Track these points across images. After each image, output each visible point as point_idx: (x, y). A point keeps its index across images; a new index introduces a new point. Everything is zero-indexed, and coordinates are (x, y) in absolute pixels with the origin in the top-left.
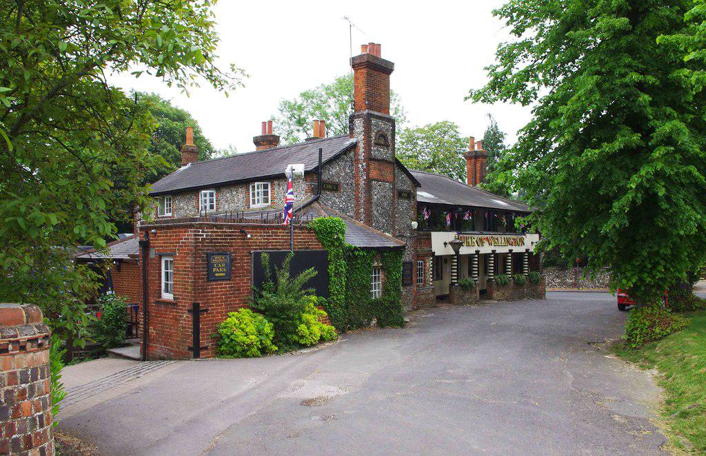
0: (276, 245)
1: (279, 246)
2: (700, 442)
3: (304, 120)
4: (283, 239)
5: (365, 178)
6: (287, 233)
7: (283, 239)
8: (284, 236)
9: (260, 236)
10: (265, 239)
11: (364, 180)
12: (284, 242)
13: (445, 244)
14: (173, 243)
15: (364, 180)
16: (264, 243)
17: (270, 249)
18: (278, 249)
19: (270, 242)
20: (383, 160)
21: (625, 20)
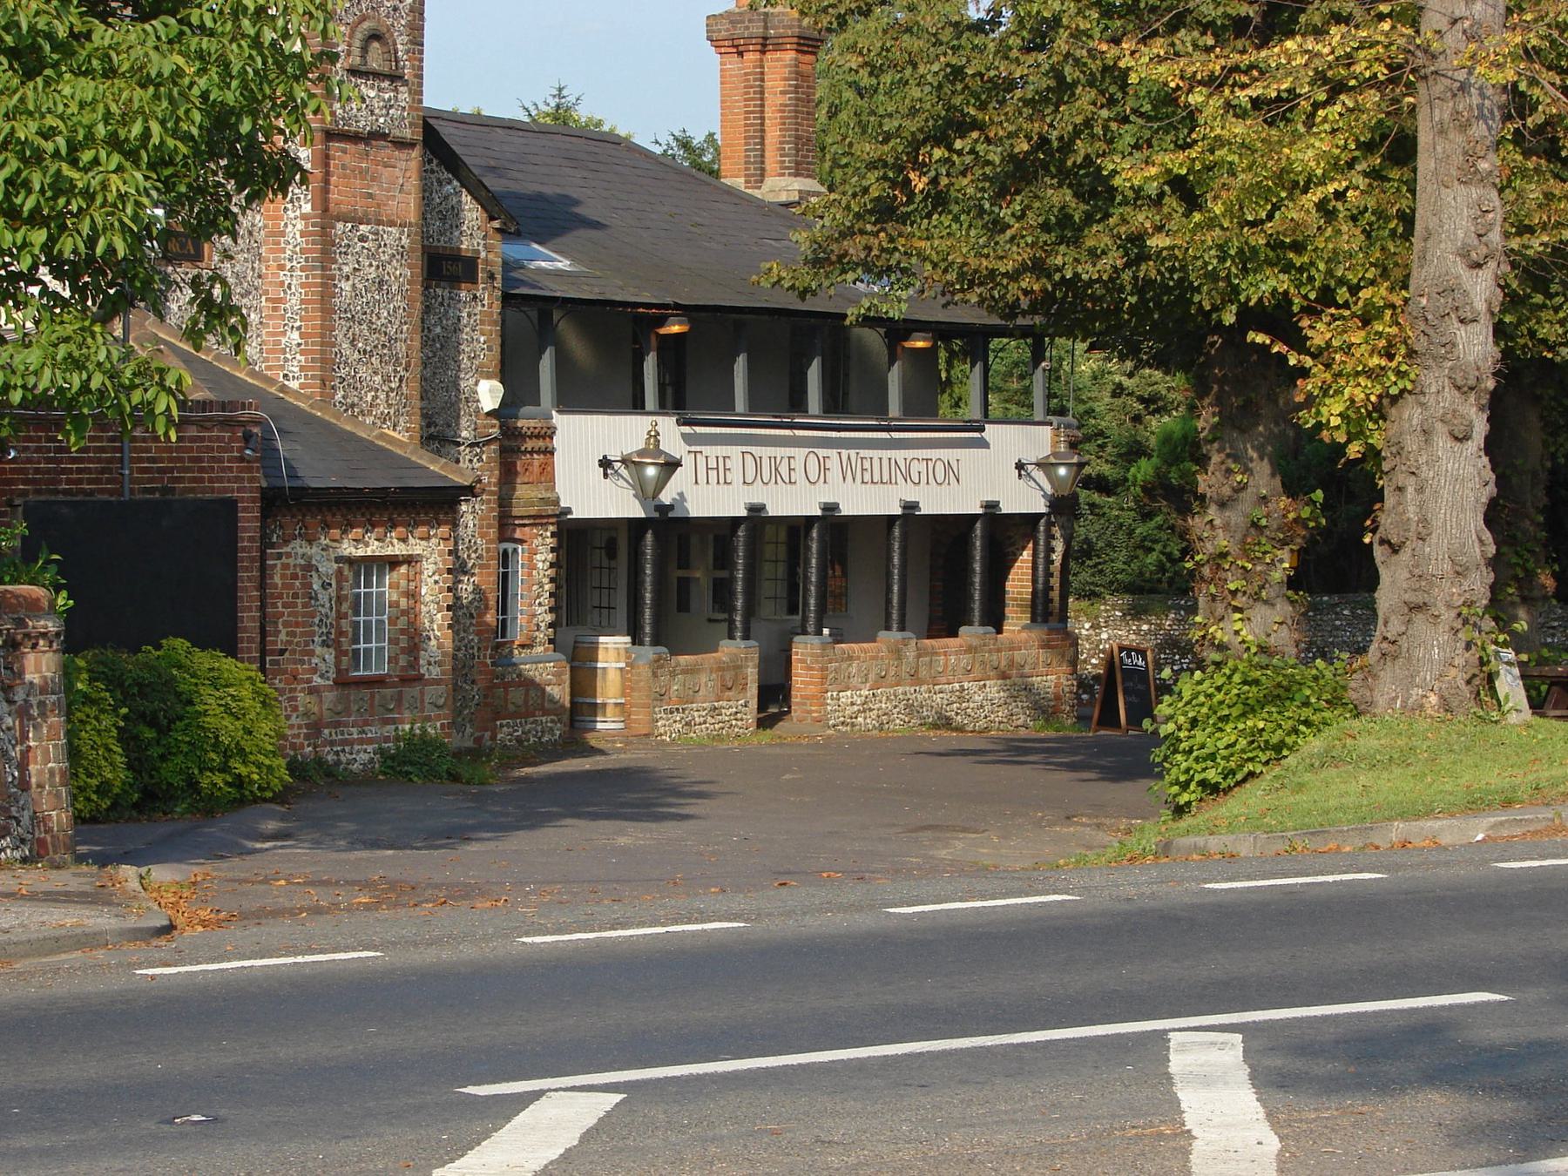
0: (80, 481)
1: (90, 481)
2: (1172, 270)
3: (1266, 504)
4: (99, 460)
5: (307, 208)
6: (112, 439)
7: (99, 460)
8: (102, 449)
9: (38, 450)
10: (48, 460)
11: (304, 217)
12: (103, 471)
13: (605, 463)
14: (212, 449)
15: (304, 217)
16: (48, 471)
17: (65, 492)
18: (83, 491)
19: (64, 471)
20: (376, 136)
21: (1182, 803)
